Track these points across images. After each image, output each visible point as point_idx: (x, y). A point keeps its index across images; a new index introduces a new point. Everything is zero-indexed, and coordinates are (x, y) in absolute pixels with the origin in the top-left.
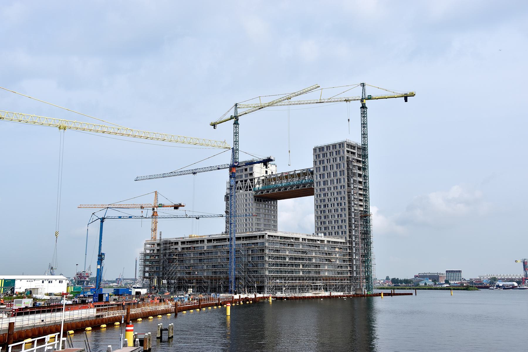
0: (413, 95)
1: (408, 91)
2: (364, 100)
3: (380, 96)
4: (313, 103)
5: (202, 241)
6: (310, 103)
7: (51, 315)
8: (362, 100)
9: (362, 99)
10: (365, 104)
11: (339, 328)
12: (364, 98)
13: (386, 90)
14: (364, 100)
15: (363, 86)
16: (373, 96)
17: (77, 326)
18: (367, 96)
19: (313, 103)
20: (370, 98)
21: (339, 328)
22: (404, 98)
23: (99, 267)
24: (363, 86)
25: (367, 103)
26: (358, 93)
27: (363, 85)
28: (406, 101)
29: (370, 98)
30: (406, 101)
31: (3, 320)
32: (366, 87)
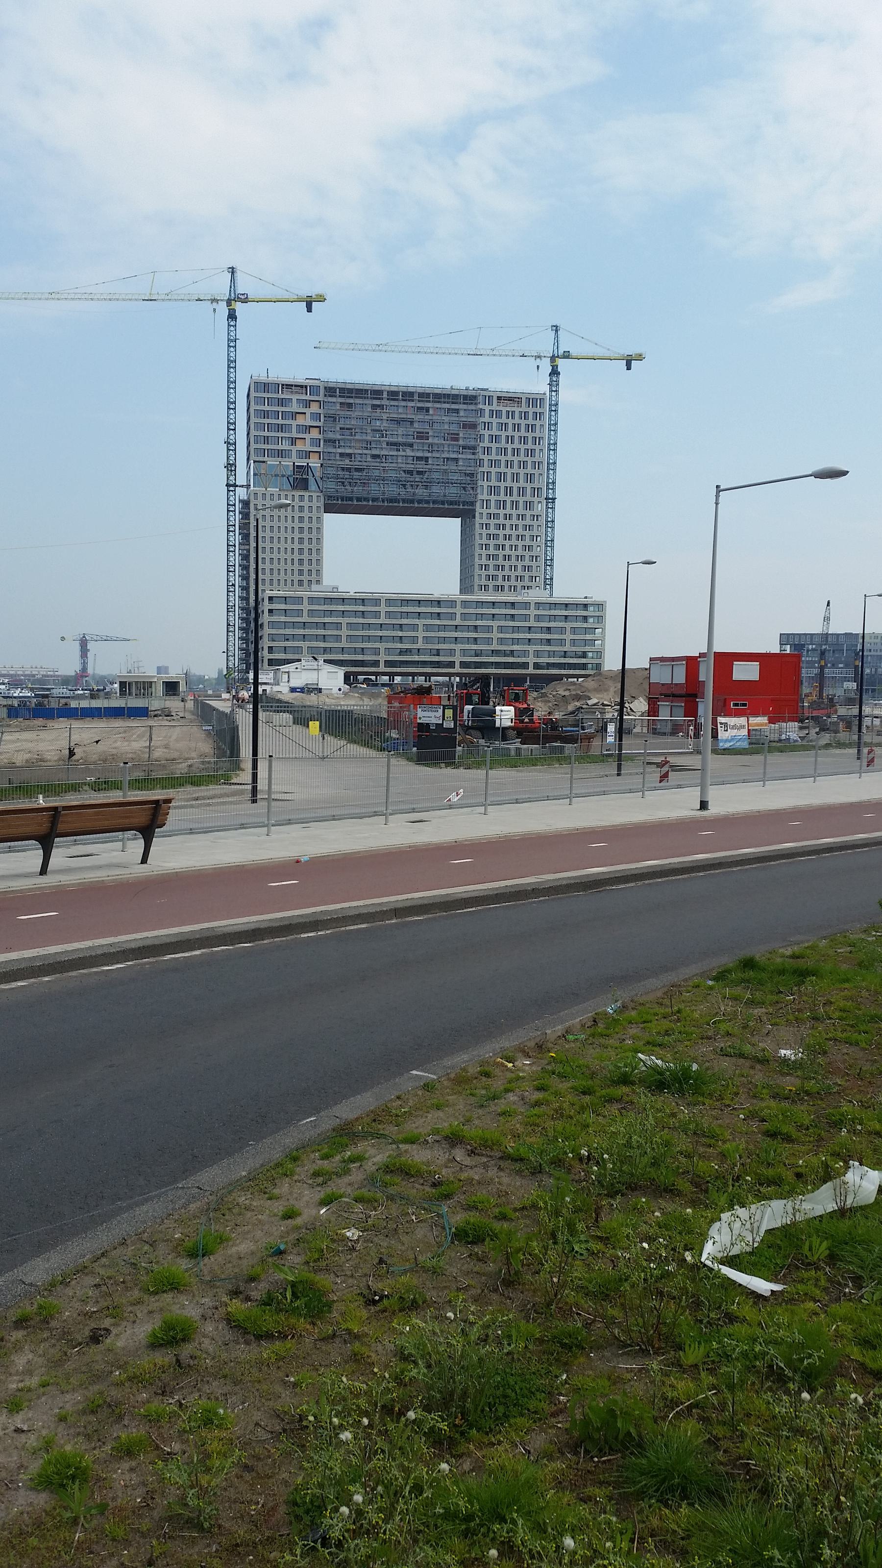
1: (313, 292)
2: (233, 302)
5: (377, 602)
8: (229, 302)
9: (553, 356)
10: (234, 310)
12: (556, 355)
13: (596, 344)
14: (233, 302)
15: (557, 331)
16: (573, 353)
17: (559, 760)
18: (561, 352)
20: (567, 356)
22: (625, 361)
23: (380, 685)
24: (557, 331)
27: (556, 329)
28: (309, 309)
29: (567, 356)
30: (309, 309)
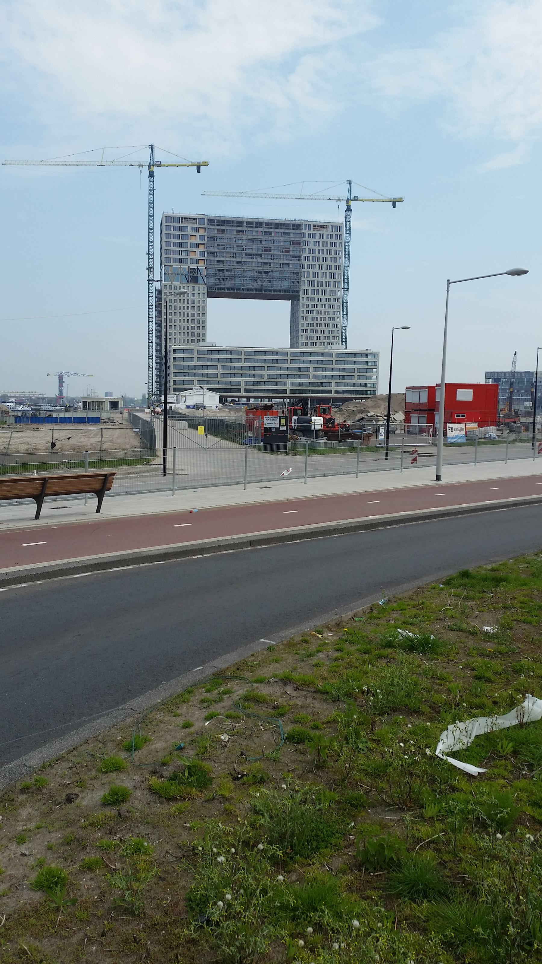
0: (206, 164)
1: (396, 196)
3: (366, 198)
4: (93, 165)
6: (89, 165)
7: (12, 442)
8: (149, 167)
10: (153, 172)
11: (415, 616)
15: (350, 184)
16: (360, 197)
18: (352, 197)
19: (93, 165)
20: (356, 199)
21: (415, 616)
24: (350, 184)
25: (155, 169)
26: (146, 159)
28: (199, 171)
29: (356, 199)
30: (199, 171)
31: (360, 460)
32: (155, 150)
